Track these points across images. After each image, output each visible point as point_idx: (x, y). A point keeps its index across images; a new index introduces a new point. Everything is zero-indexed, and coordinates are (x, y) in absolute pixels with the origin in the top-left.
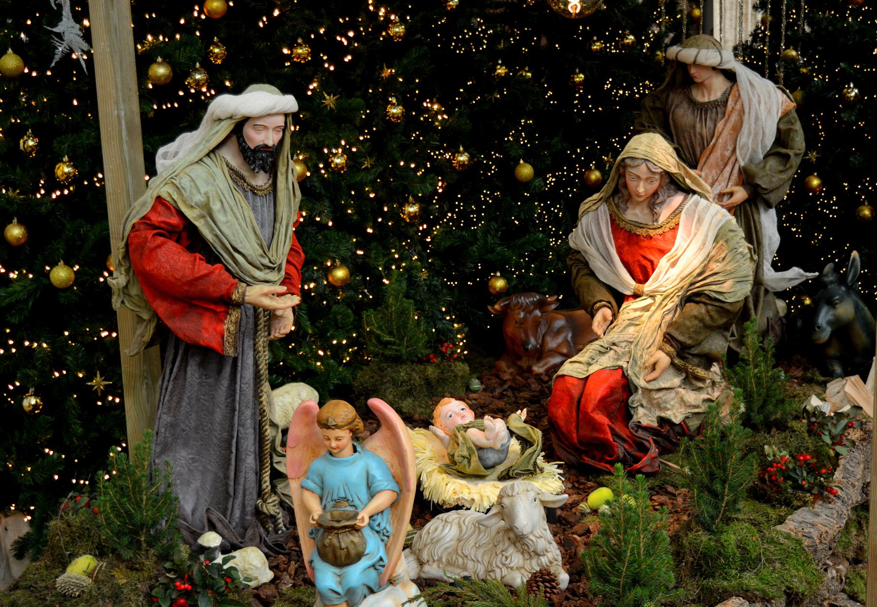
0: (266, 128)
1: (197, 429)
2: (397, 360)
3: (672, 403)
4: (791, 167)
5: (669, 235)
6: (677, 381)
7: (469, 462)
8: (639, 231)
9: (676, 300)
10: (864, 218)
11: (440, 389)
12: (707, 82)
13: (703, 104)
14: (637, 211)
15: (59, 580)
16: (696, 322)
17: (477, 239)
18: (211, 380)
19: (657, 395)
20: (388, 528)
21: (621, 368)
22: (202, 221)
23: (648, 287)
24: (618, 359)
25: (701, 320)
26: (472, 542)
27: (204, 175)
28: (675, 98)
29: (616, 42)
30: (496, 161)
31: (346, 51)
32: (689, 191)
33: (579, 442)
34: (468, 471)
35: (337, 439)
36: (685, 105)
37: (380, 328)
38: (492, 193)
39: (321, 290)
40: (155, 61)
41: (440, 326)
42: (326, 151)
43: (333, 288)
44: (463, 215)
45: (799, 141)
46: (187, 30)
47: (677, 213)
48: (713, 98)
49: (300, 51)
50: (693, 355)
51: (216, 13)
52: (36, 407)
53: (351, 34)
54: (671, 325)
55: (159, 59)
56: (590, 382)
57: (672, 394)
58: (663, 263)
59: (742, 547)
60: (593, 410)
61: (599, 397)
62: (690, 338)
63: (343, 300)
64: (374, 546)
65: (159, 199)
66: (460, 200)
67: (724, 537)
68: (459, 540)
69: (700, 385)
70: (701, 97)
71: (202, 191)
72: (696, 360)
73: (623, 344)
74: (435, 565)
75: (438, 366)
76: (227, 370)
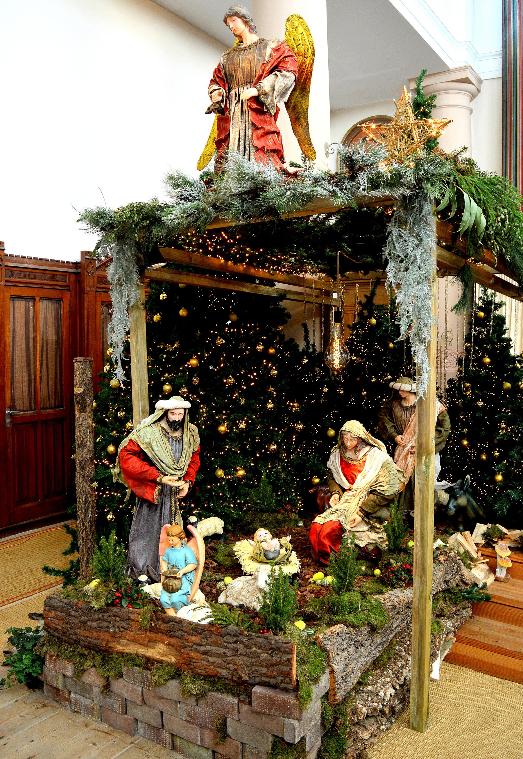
0: (176, 414)
1: (147, 533)
2: (262, 511)
3: (364, 538)
4: (442, 436)
5: (362, 464)
6: (366, 528)
7: (260, 556)
8: (350, 462)
9: (365, 493)
10: (483, 459)
11: (283, 525)
12: (407, 398)
13: (406, 407)
14: (350, 453)
15: (84, 588)
16: (373, 503)
17: (310, 461)
18: (153, 513)
19: (357, 534)
20: (192, 579)
21: (339, 521)
22: (147, 449)
23: (354, 486)
24: (339, 517)
25: (375, 502)
26: (246, 590)
27: (150, 431)
28: (395, 404)
29: (383, 378)
30: (318, 428)
31: (252, 381)
32: (372, 446)
33: (319, 552)
34: (259, 560)
35: (172, 541)
36: (399, 407)
37: (255, 496)
38: (318, 442)
39: (234, 479)
40: (165, 384)
41: (290, 497)
42: (237, 422)
43: (240, 479)
44: (305, 450)
45: (448, 424)
46: (183, 372)
47: (365, 455)
48: (410, 405)
49: (230, 381)
50: (373, 517)
51: (194, 365)
52: (112, 519)
53: (255, 374)
54: (363, 503)
55: (167, 383)
56: (324, 527)
57: (364, 534)
58: (359, 476)
59: (350, 602)
60: (324, 538)
61: (326, 533)
62: (370, 509)
63: (244, 484)
64: (186, 586)
65: (131, 439)
66: (304, 444)
67: (342, 597)
68: (242, 588)
69: (378, 531)
70: (406, 404)
71: (148, 438)
72: (375, 520)
73: (341, 511)
74: (231, 598)
75: (283, 514)
76: (159, 510)
